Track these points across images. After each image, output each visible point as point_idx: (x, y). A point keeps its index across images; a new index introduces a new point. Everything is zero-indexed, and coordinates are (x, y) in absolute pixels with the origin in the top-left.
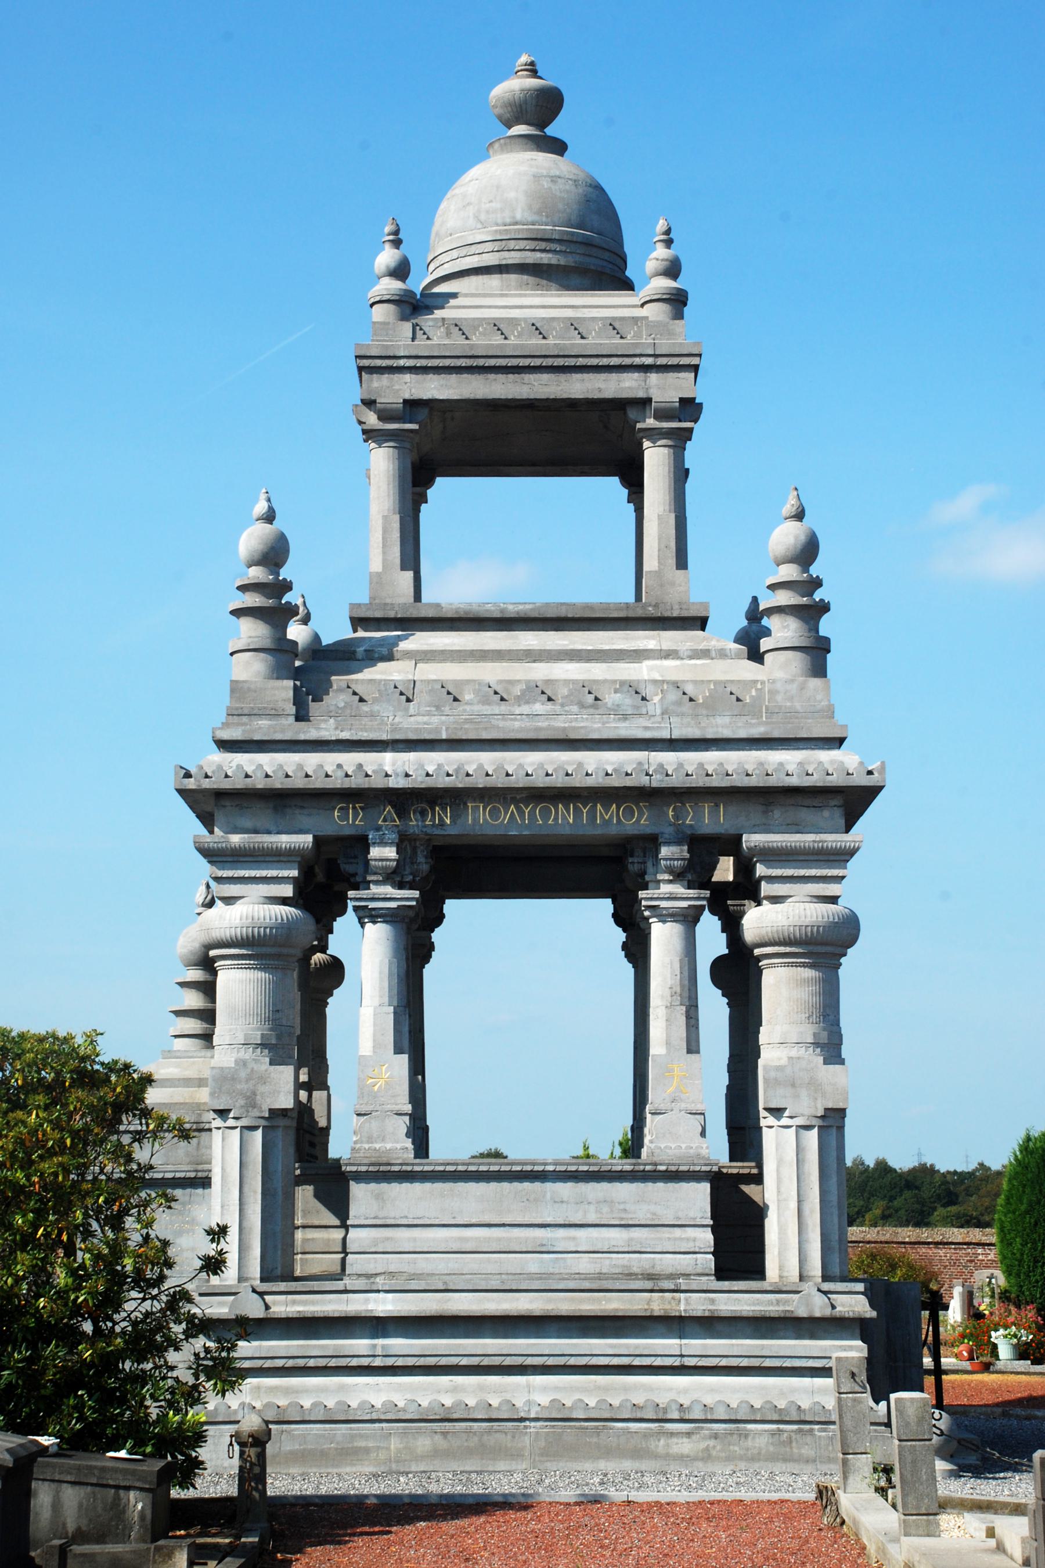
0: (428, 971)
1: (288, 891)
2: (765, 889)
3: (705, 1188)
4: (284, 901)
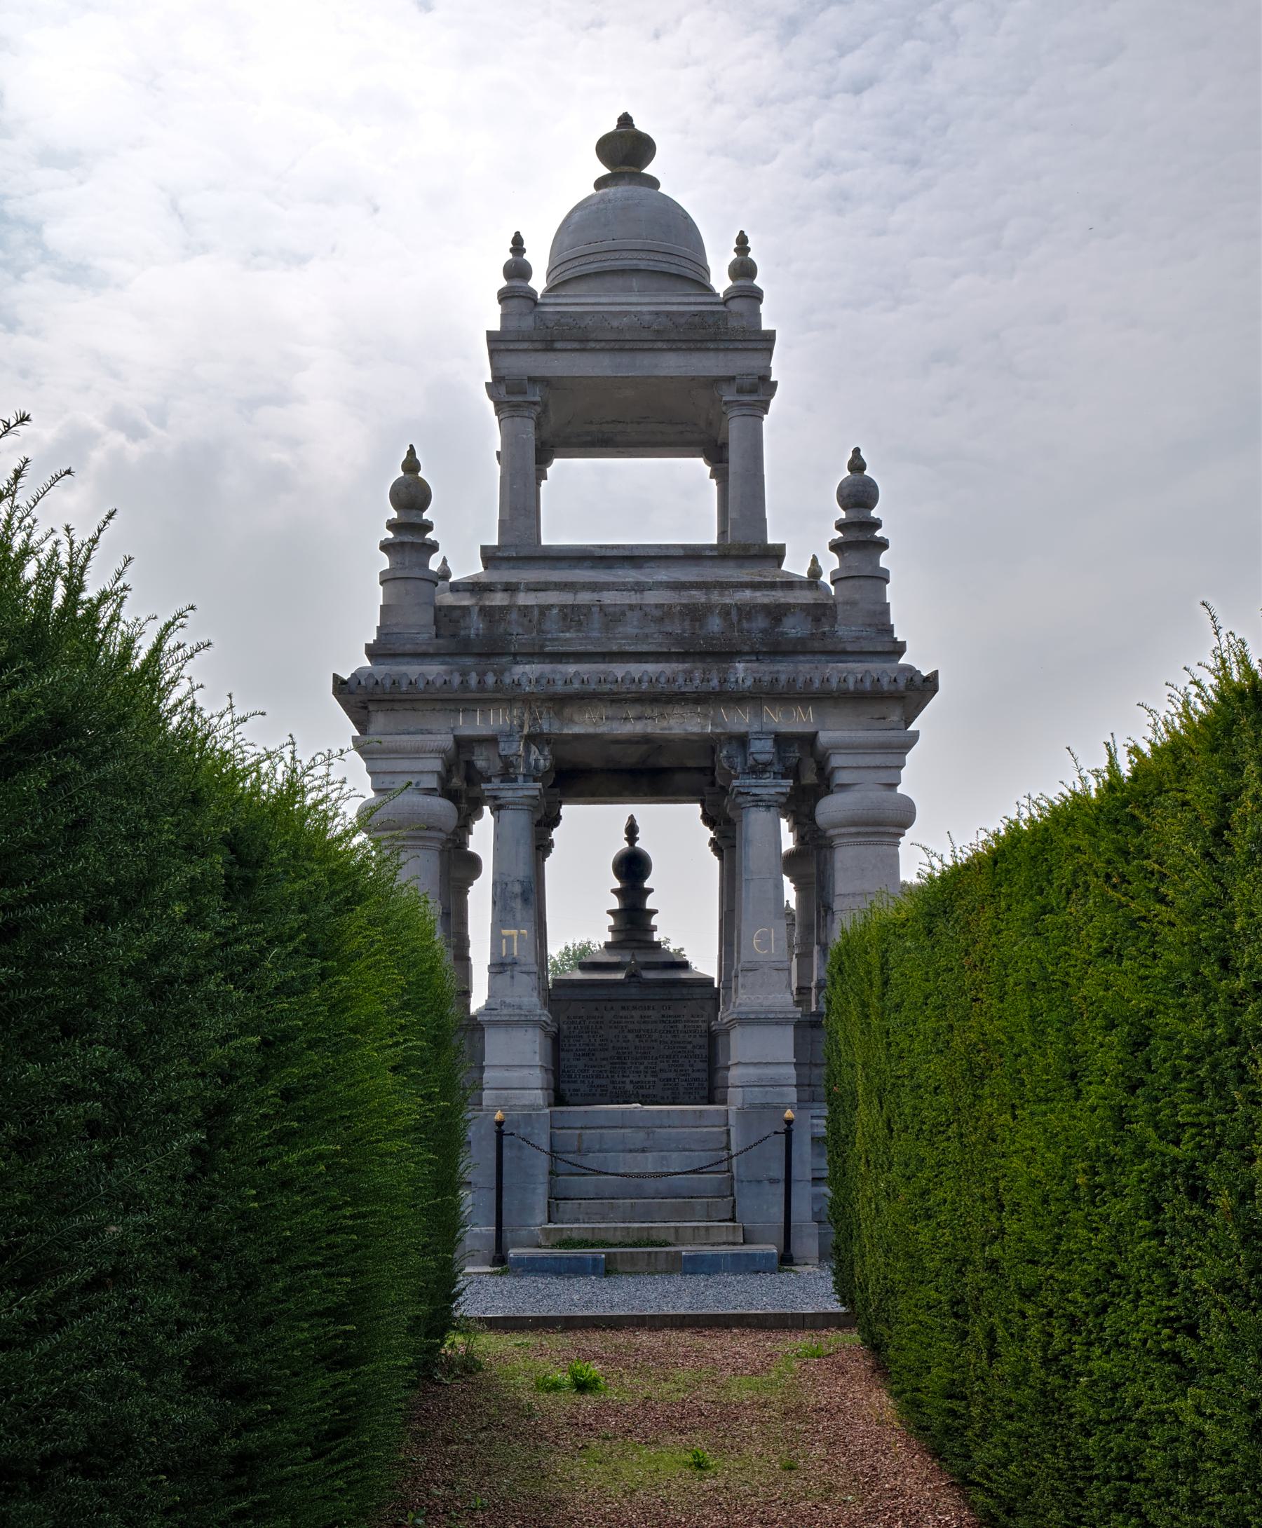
0: (549, 863)
1: (433, 782)
2: (842, 777)
3: (789, 1032)
4: (429, 792)
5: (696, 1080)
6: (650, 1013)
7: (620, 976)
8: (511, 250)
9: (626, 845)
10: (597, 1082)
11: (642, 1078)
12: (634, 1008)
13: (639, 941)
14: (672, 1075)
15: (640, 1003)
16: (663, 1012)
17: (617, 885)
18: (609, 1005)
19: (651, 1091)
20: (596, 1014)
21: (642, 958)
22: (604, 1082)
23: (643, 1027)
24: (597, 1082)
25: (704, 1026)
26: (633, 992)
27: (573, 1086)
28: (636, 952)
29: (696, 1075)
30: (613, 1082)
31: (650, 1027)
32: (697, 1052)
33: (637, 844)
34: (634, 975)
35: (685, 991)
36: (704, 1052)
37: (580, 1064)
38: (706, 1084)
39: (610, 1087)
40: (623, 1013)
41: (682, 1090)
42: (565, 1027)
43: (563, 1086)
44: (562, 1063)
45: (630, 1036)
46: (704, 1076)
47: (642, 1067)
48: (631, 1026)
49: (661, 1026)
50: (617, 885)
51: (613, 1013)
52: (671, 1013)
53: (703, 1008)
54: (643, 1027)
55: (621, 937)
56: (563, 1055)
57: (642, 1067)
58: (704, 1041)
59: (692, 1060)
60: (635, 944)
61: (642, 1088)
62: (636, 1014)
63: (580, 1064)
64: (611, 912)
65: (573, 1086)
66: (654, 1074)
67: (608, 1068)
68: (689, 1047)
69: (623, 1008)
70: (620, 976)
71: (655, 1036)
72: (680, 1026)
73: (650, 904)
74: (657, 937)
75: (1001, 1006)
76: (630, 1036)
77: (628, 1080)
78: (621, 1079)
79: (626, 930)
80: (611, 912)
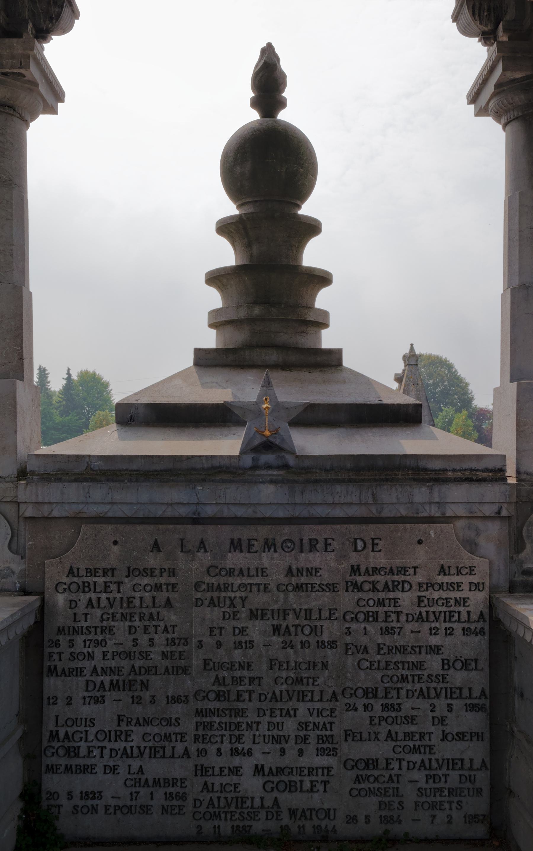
5: (453, 763)
6: (315, 559)
7: (227, 445)
8: (256, 103)
9: (254, 116)
10: (155, 768)
11: (290, 758)
12: (269, 545)
13: (284, 348)
14: (380, 750)
15: (286, 531)
16: (354, 559)
17: (230, 209)
18: (193, 533)
19: (316, 800)
20: (153, 561)
21: (295, 391)
22: (178, 769)
23: (294, 600)
24: (155, 768)
25: (477, 600)
26: (268, 496)
27: (81, 783)
28: (276, 376)
29: (450, 750)
30: (202, 771)
31: (317, 600)
32: (457, 677)
33: (283, 116)
34: (268, 446)
35: (420, 494)
36: (478, 680)
37: (105, 715)
38: (482, 779)
39: (194, 787)
40: (235, 560)
41: (409, 794)
42: (61, 599)
43: (52, 782)
44: (50, 712)
45: (257, 630)
46: (476, 752)
47: (290, 726)
48: (258, 600)
49: (347, 600)
50: (230, 209)
51: (205, 558)
52: (379, 559)
53: (472, 546)
54: (294, 600)
55: (237, 337)
56: (52, 685)
57: (290, 726)
58: (475, 646)
59: (441, 703)
60: (274, 356)
61: (291, 787)
62: (275, 563)
63: (105, 715)
64: (216, 278)
65: (81, 783)
66: (327, 746)
67: (189, 726)
68: (434, 664)
69: (236, 545)
70: (227, 445)
71: (331, 630)
72: (406, 599)
73: (313, 255)
74: (328, 340)
75: (216, 823)
76: (257, 630)
77: (247, 764)
78: (223, 761)
79: (251, 321)
80: (216, 278)
